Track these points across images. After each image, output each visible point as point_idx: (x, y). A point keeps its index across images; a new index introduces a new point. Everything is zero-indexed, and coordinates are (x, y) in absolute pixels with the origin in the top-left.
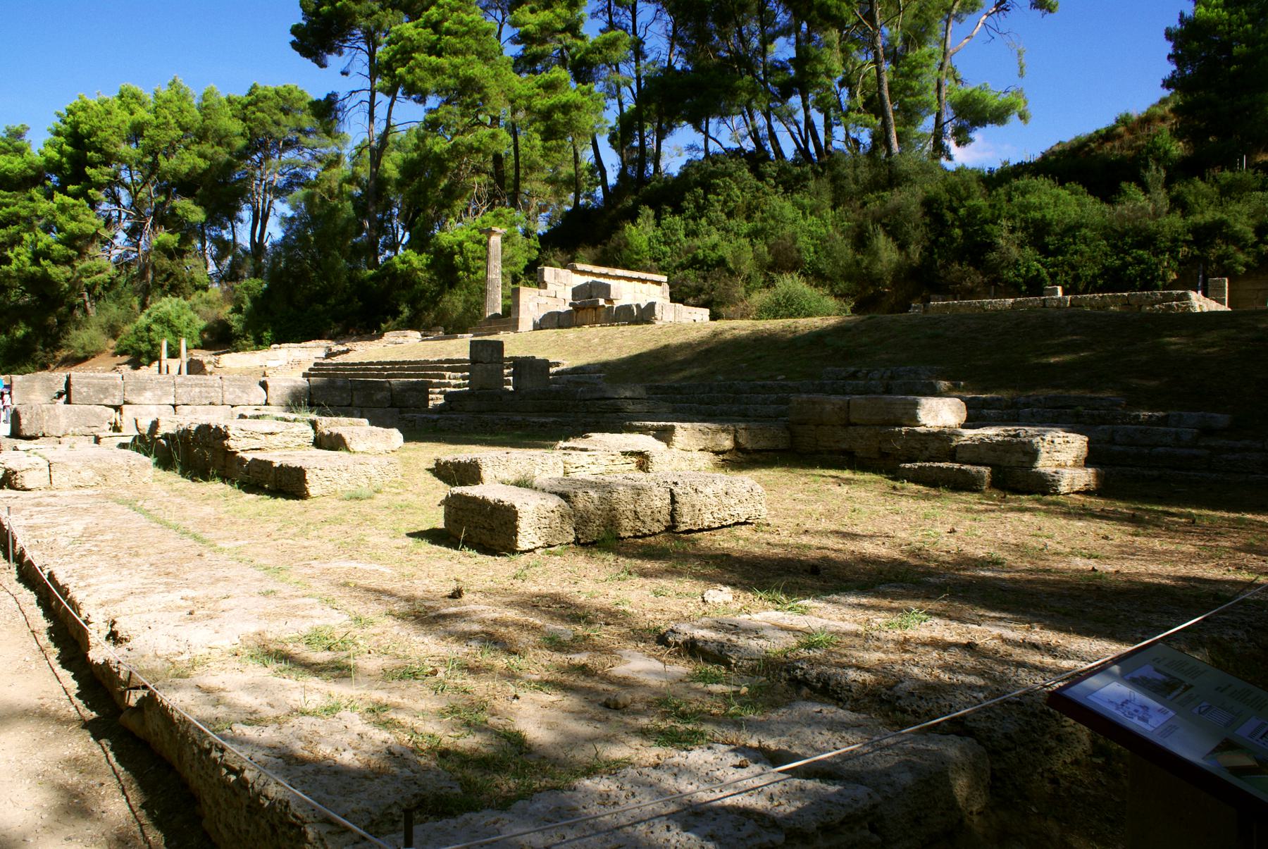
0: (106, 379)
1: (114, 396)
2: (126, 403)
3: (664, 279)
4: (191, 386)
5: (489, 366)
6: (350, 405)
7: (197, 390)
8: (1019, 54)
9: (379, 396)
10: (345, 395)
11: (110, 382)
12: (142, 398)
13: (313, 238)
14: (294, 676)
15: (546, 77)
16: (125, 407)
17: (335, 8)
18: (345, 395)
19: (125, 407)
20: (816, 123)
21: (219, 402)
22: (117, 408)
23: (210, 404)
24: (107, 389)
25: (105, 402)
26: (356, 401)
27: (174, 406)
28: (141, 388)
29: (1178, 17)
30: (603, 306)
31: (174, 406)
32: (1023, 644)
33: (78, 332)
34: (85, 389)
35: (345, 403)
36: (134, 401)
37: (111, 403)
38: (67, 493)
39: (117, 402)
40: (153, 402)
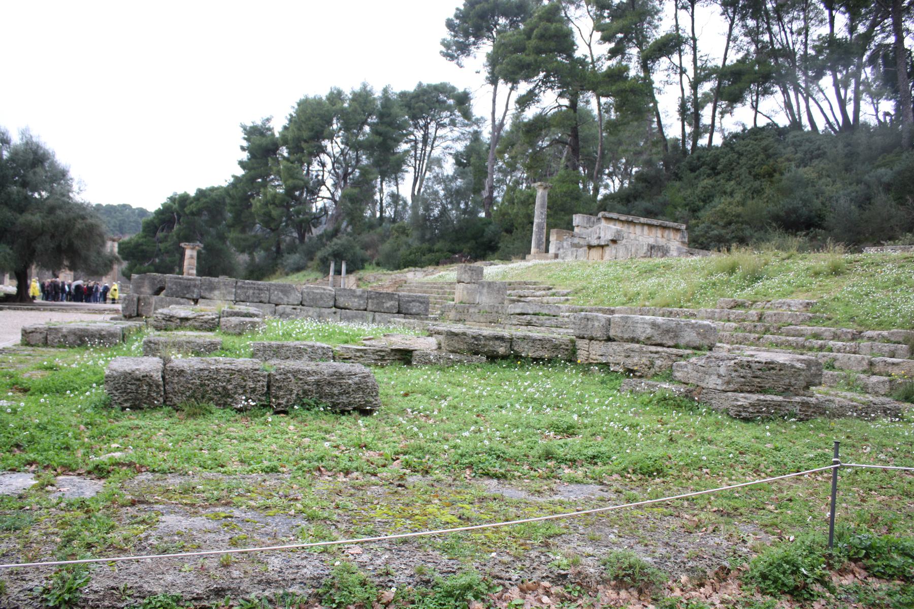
1: (193, 292)
3: (684, 227)
4: (247, 288)
5: (469, 286)
6: (365, 310)
7: (251, 291)
9: (389, 304)
10: (362, 302)
11: (192, 282)
13: (36, 195)
14: (148, 415)
18: (362, 302)
21: (266, 301)
24: (189, 287)
25: (187, 296)
26: (370, 307)
29: (268, 116)
32: (211, 348)
33: (288, 256)
35: (362, 308)
37: (191, 297)
38: (686, 516)
39: (195, 296)
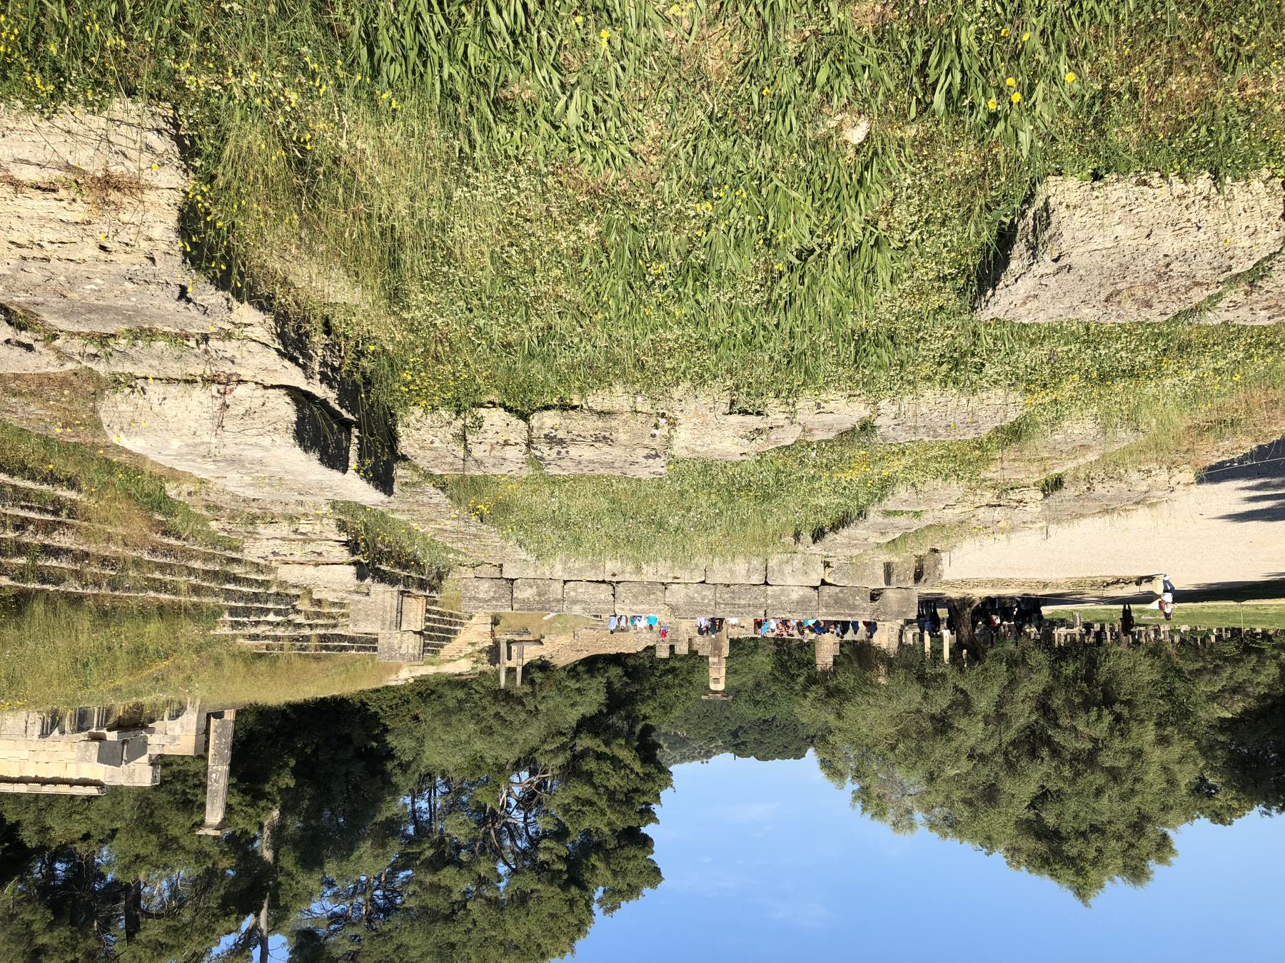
0: (836, 614)
2: (816, 588)
7: (742, 602)
8: (1036, 296)
10: (573, 594)
12: (801, 593)
15: (558, 91)
16: (818, 584)
17: (34, 565)
19: (818, 584)
20: (357, 498)
22: (824, 583)
23: (728, 586)
25: (838, 589)
27: (766, 583)
28: (802, 603)
30: (109, 730)
31: (766, 583)
34: (857, 603)
35: (571, 584)
36: (808, 590)
40: (790, 588)
